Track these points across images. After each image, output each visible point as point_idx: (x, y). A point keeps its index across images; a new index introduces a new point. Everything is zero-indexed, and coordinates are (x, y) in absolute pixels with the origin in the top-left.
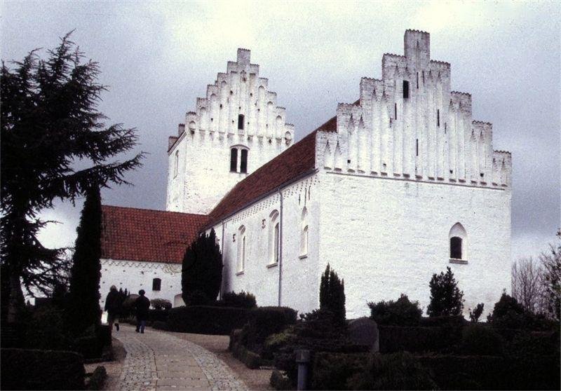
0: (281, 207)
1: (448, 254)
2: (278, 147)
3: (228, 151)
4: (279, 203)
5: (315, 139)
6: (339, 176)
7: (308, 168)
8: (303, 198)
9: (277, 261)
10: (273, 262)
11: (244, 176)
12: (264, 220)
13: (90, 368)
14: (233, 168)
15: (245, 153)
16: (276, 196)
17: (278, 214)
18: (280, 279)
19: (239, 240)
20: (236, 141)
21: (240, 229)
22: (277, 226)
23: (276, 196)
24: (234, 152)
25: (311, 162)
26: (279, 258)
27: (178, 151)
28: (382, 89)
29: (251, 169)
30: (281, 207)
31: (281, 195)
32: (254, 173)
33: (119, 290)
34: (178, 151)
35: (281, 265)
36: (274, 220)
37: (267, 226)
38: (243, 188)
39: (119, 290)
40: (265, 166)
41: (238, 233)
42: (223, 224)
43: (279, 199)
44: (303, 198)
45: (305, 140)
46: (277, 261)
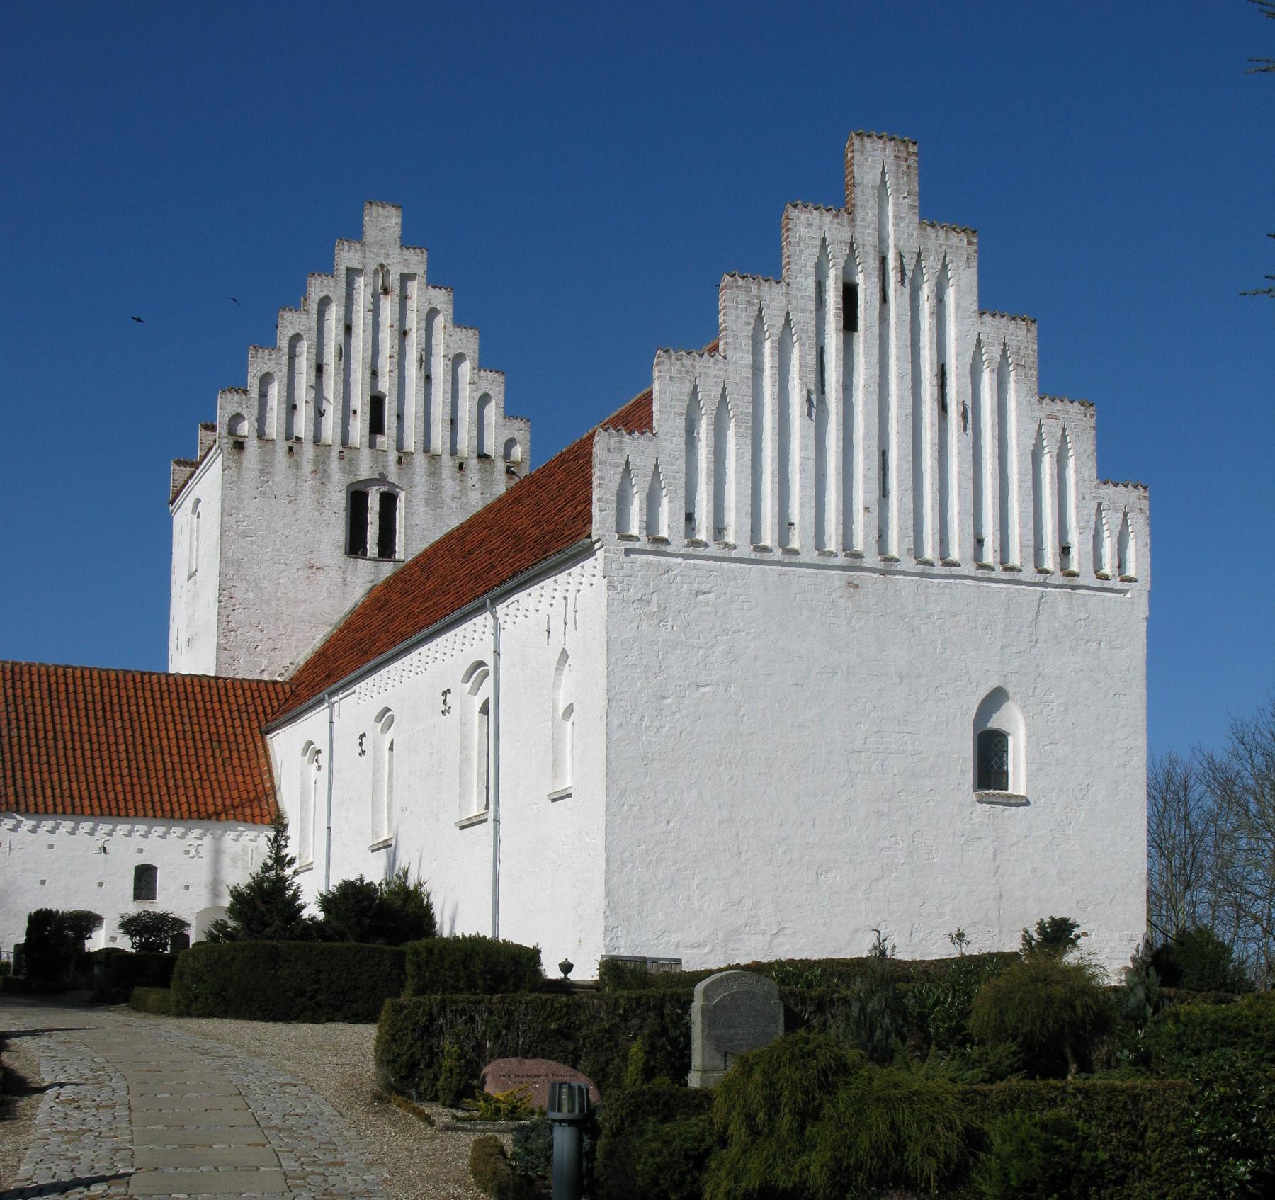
0: (497, 653)
1: (969, 778)
2: (487, 482)
3: (338, 499)
4: (489, 638)
5: (590, 455)
6: (662, 559)
7: (575, 537)
8: (556, 625)
9: (487, 807)
10: (475, 810)
11: (387, 569)
12: (363, 736)
13: (21, 977)
14: (355, 546)
15: (388, 502)
16: (479, 620)
17: (487, 674)
18: (496, 859)
19: (376, 749)
20: (365, 471)
21: (305, 752)
22: (484, 710)
23: (482, 622)
24: (357, 500)
25: (579, 523)
26: (492, 796)
27: (198, 501)
28: (784, 304)
29: (407, 547)
30: (497, 653)
31: (496, 619)
32: (416, 561)
33: (461, 937)
34: (198, 501)
35: (497, 821)
36: (475, 691)
37: (456, 711)
38: (387, 602)
39: (461, 937)
40: (449, 537)
41: (373, 729)
42: (332, 706)
43: (489, 630)
44: (556, 625)
45: (562, 459)
46: (487, 807)
